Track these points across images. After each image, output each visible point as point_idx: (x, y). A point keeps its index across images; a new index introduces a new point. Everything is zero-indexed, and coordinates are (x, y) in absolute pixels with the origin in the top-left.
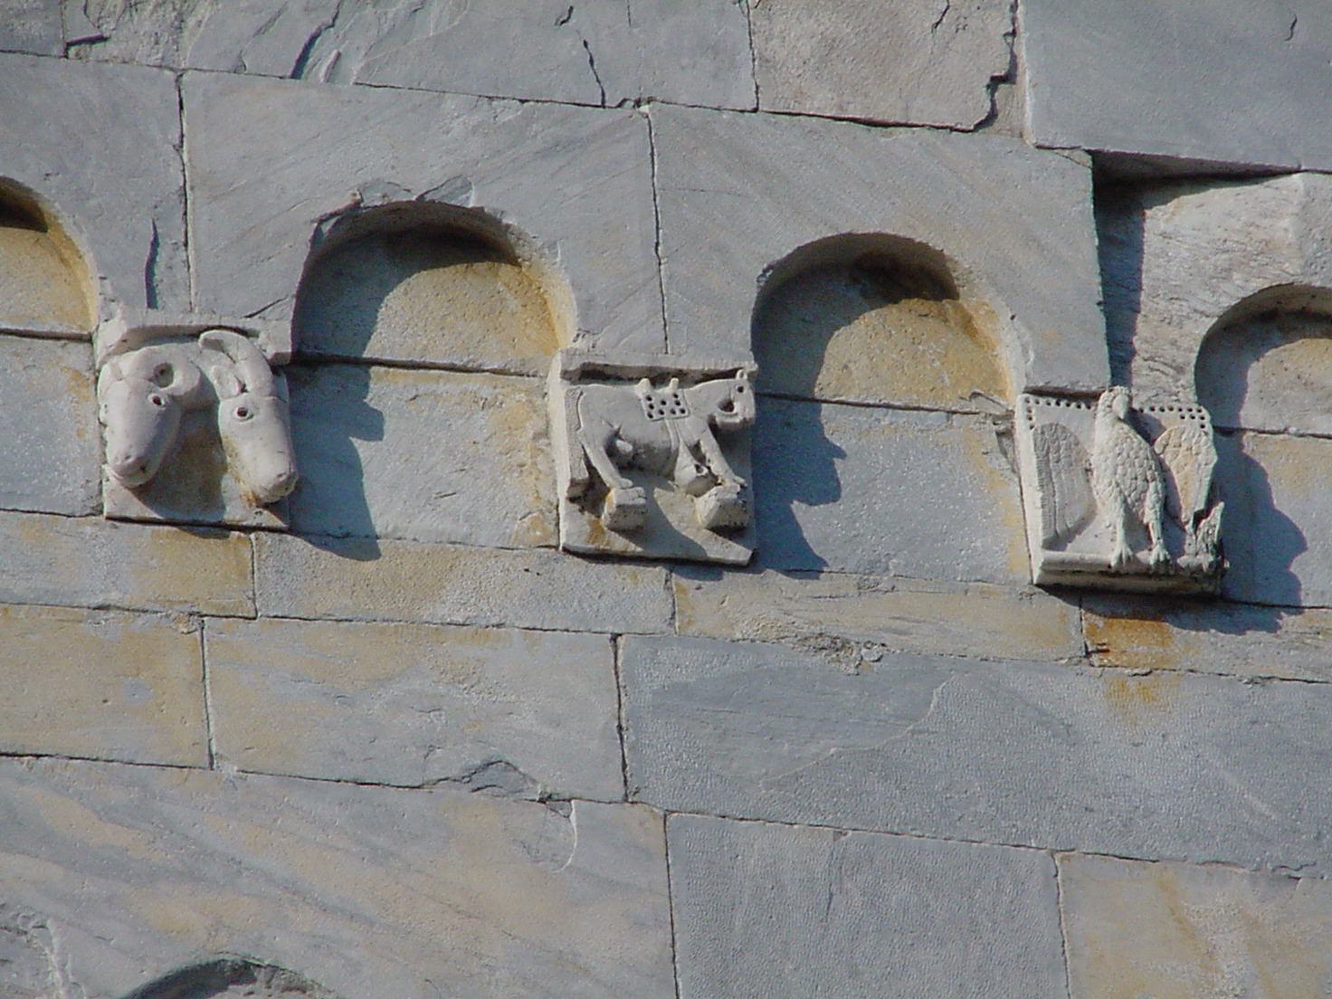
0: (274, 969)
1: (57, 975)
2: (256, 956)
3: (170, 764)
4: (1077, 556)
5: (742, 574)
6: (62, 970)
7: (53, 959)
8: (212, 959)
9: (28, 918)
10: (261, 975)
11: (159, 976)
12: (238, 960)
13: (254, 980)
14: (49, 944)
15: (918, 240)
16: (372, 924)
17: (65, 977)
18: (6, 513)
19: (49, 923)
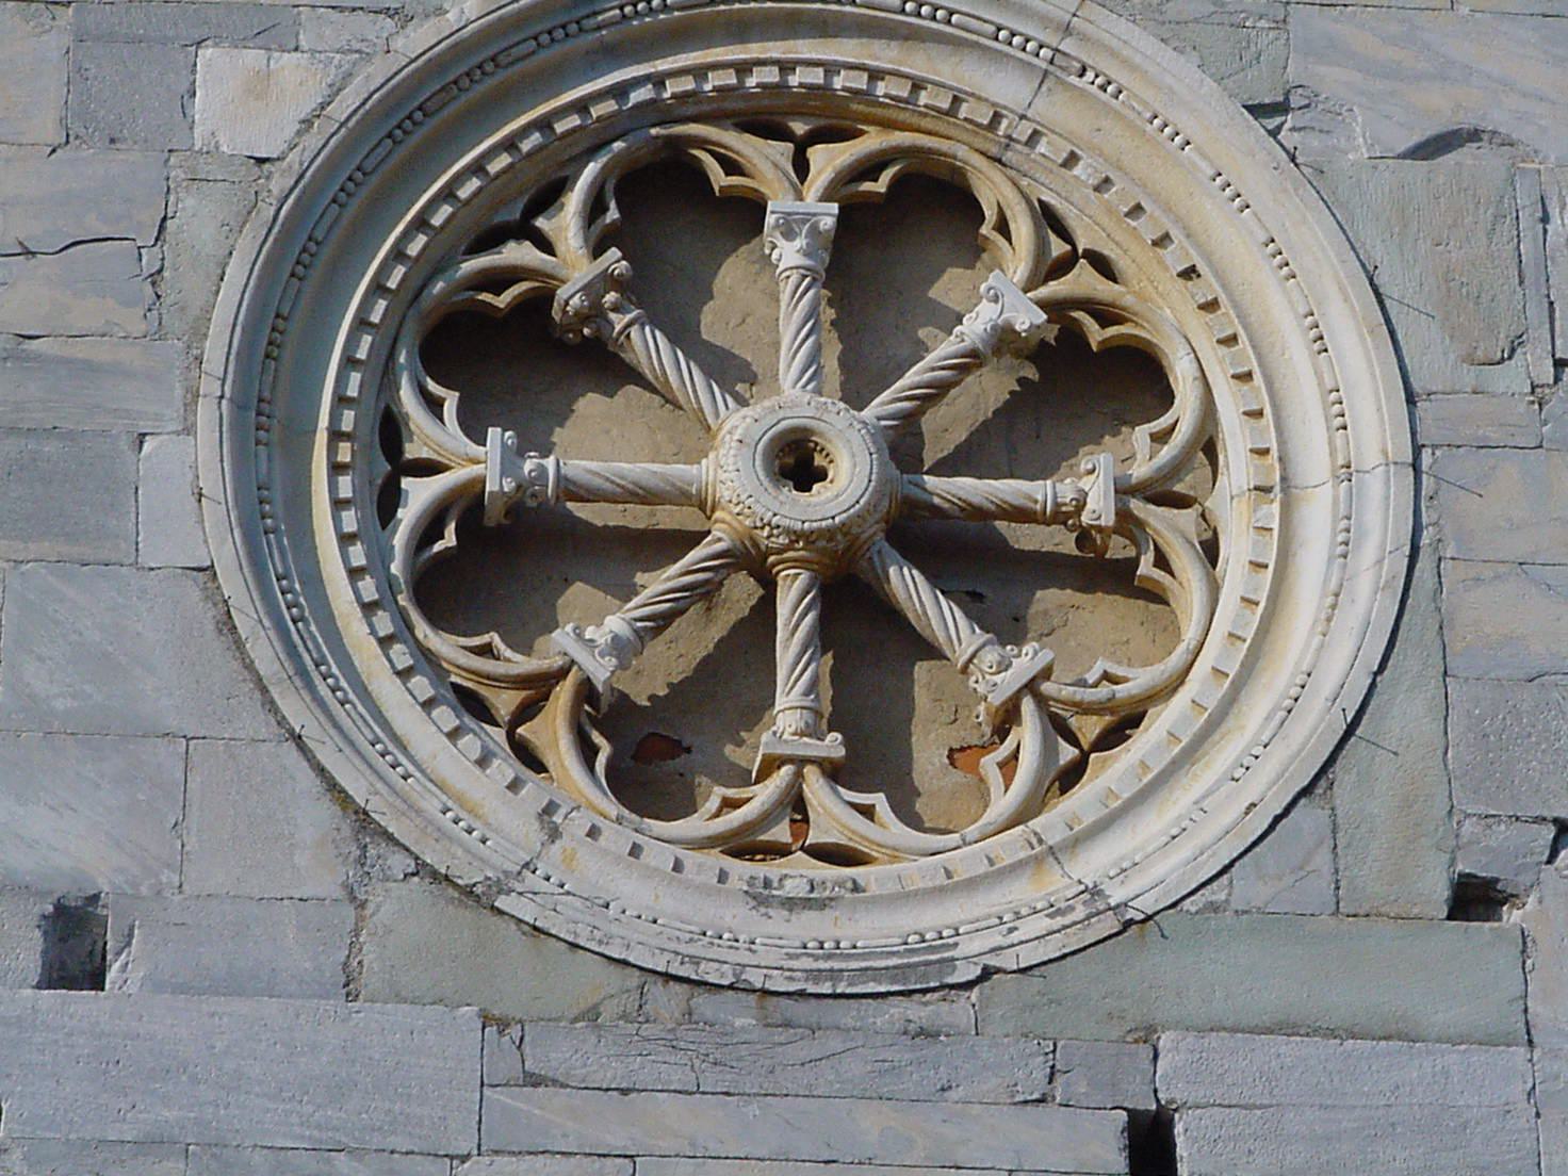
0: (1494, 133)
1: (1361, 140)
2: (1482, 125)
3: (390, 342)
4: (772, 839)
5: (531, 264)
6: (1364, 137)
7: (1358, 129)
8: (1455, 127)
9: (1342, 105)
10: (1485, 137)
11: (1423, 139)
12: (1472, 127)
13: (1481, 140)
14: (1355, 120)
15: (990, 414)
16: (1554, 103)
17: (1366, 142)
18: (372, 89)
19: (1355, 108)
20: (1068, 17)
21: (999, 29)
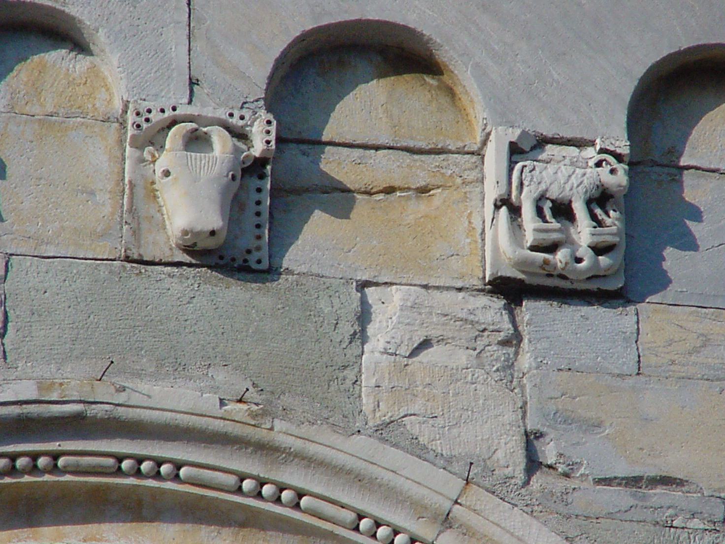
20: (447, 505)
21: (360, 517)
